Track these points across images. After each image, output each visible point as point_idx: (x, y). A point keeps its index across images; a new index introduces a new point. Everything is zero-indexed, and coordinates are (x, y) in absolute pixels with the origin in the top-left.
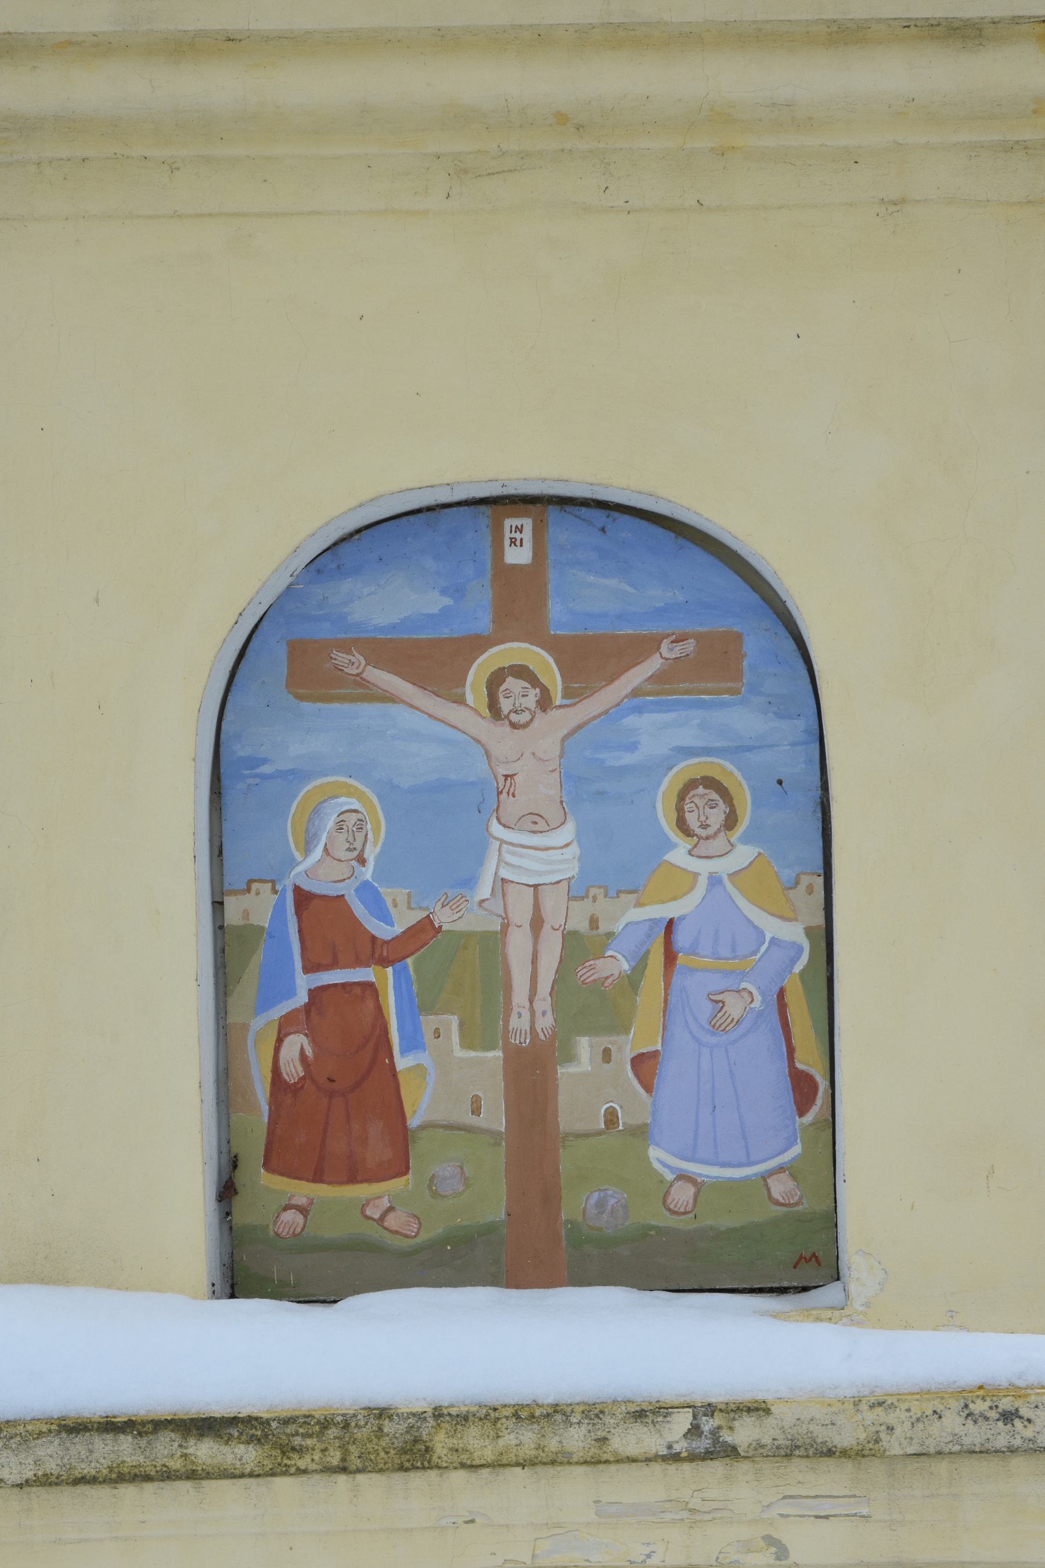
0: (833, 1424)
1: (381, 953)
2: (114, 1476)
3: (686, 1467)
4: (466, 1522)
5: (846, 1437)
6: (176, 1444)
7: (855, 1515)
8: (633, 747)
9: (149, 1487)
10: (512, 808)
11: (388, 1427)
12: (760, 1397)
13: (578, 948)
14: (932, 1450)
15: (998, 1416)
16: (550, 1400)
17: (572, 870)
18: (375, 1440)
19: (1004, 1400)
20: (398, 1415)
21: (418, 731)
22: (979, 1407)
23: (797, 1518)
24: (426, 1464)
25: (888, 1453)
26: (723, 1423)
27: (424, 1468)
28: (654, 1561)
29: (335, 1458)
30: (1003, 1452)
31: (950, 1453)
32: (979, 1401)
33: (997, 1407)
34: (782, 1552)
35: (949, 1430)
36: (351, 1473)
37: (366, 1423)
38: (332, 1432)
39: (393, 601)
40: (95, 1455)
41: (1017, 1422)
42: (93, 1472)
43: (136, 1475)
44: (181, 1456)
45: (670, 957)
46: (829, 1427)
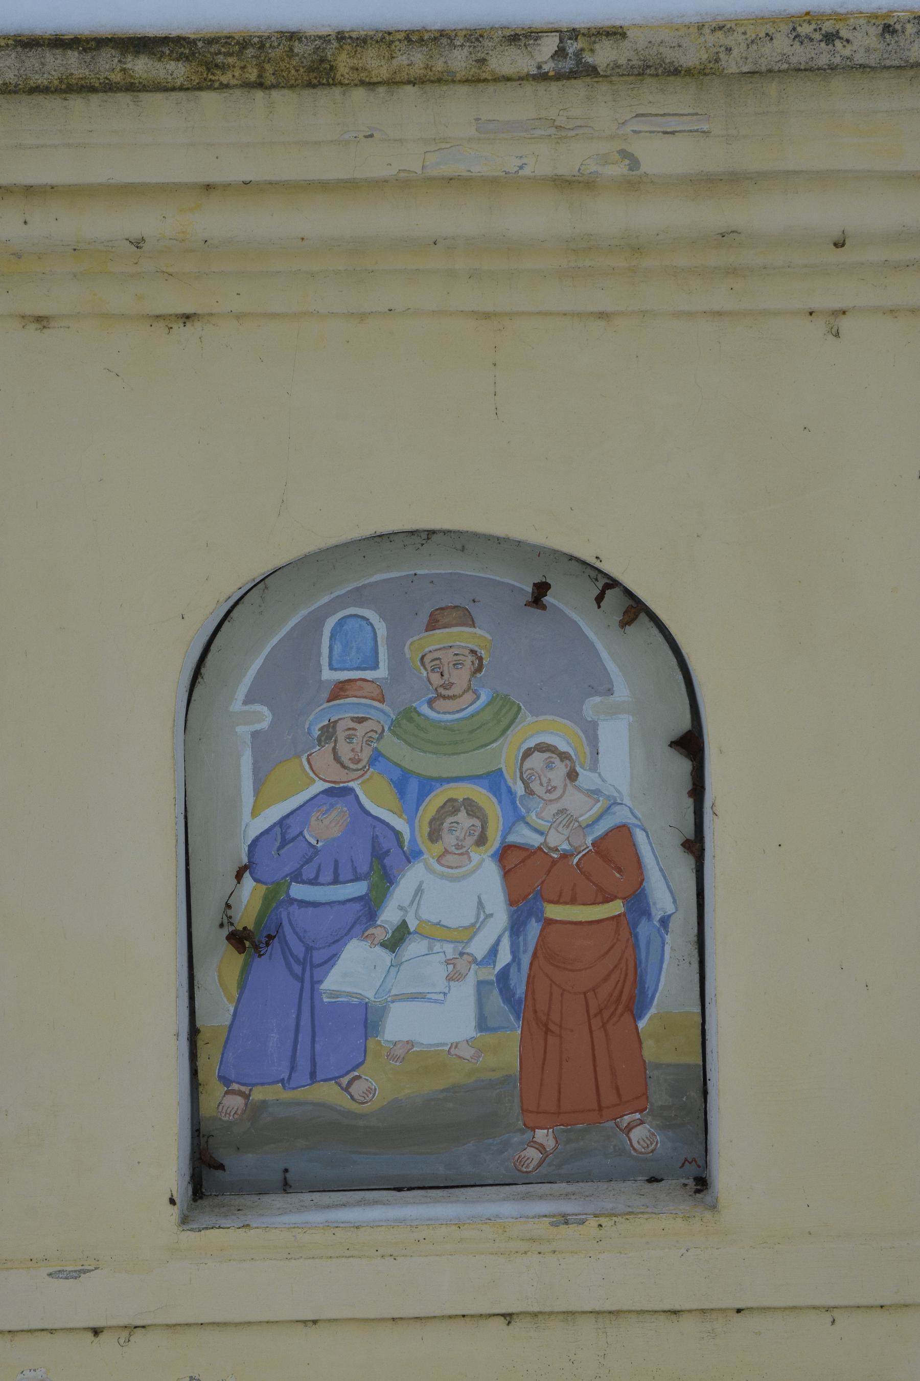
0: (680, 46)
2: (64, 86)
3: (555, 87)
4: (366, 137)
5: (690, 58)
6: (116, 60)
7: (697, 131)
9: (95, 99)
11: (298, 48)
12: (618, 23)
14: (764, 69)
15: (821, 37)
16: (437, 27)
18: (287, 60)
19: (827, 23)
20: (306, 38)
22: (805, 29)
23: (648, 134)
24: (331, 81)
25: (726, 71)
26: (585, 46)
27: (329, 85)
28: (527, 172)
29: (252, 75)
30: (825, 70)
31: (779, 71)
32: (805, 25)
33: (820, 29)
34: (634, 163)
35: (779, 51)
36: (266, 88)
37: (279, 45)
38: (250, 52)
40: (46, 67)
41: (838, 43)
42: (46, 83)
43: (82, 86)
44: (121, 71)
46: (677, 48)
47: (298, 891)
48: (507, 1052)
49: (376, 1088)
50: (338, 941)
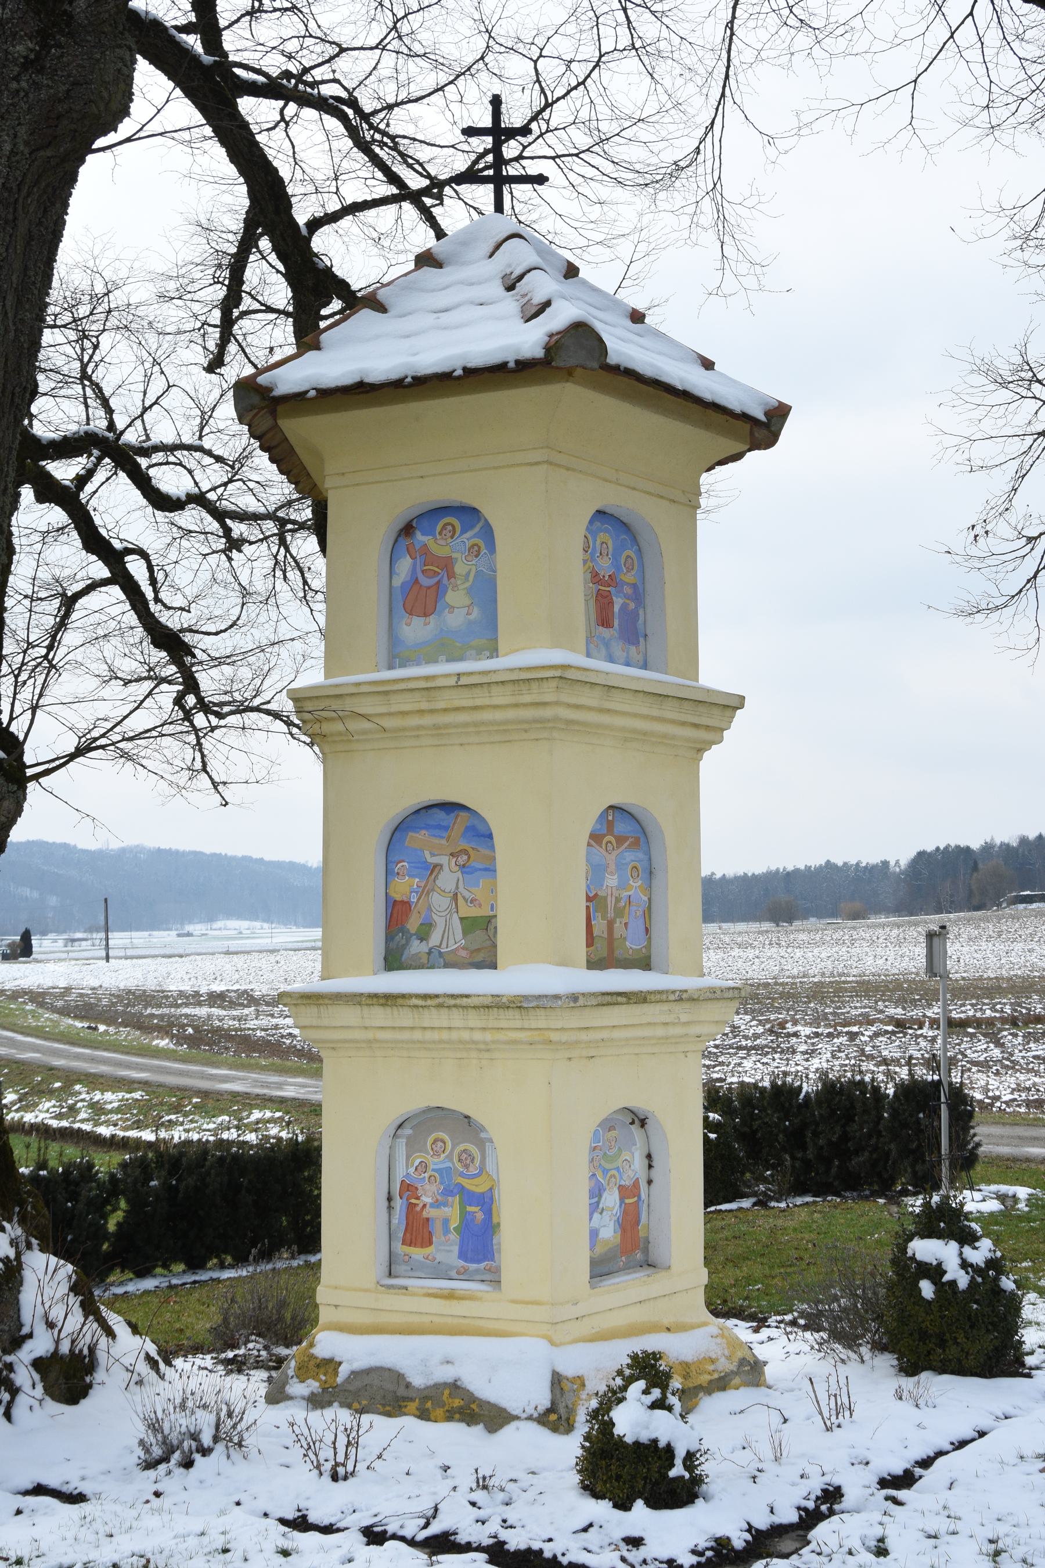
13: (618, 900)
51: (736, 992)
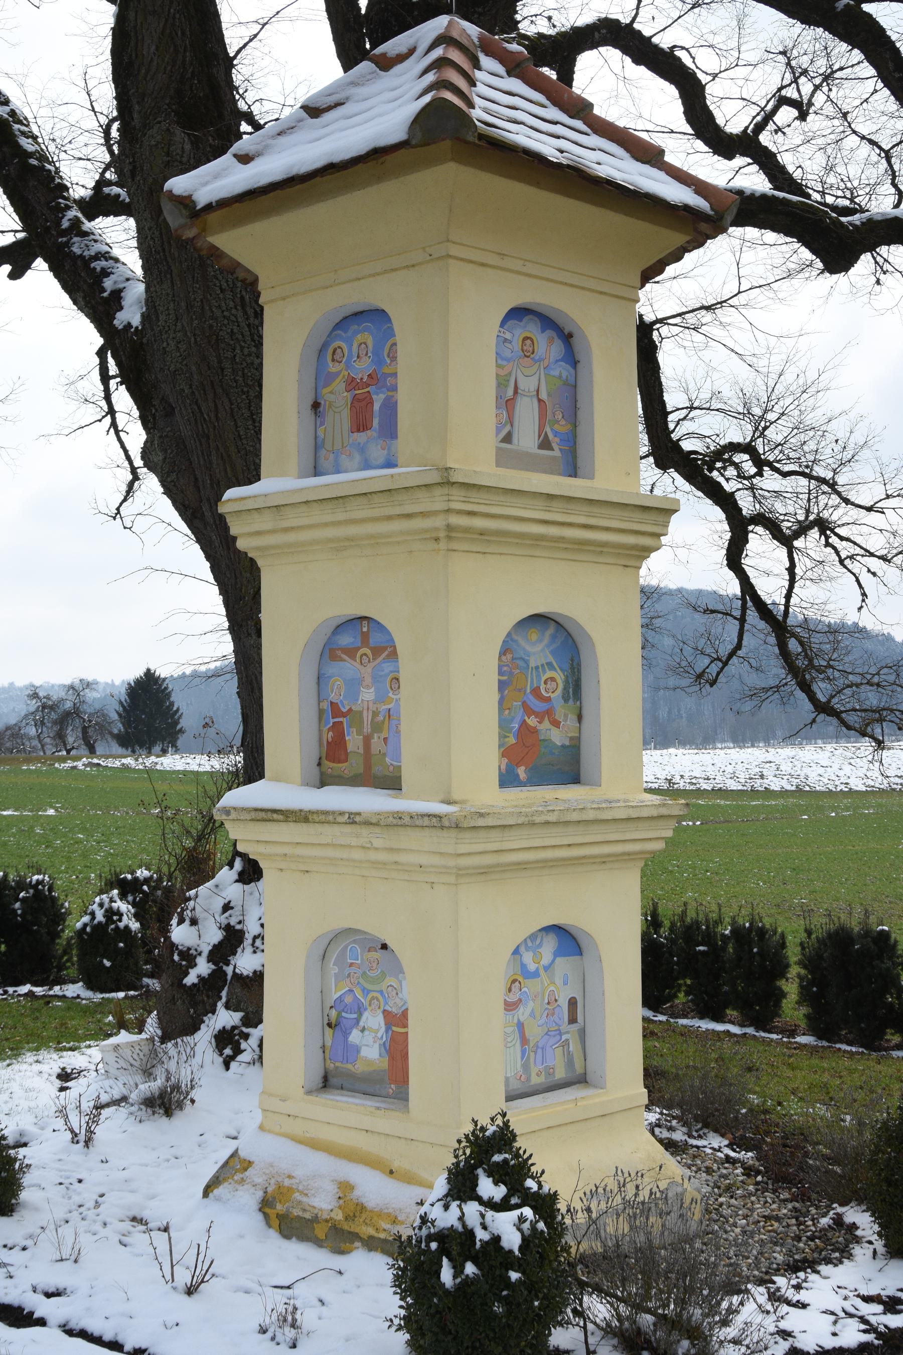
1: (344, 715)
5: (374, 821)
8: (383, 671)
10: (364, 683)
13: (375, 714)
17: (373, 698)
21: (349, 667)
39: (346, 640)
45: (389, 717)
47: (344, 1014)
48: (385, 1064)
49: (359, 1068)
50: (352, 1028)
51: (434, 820)
